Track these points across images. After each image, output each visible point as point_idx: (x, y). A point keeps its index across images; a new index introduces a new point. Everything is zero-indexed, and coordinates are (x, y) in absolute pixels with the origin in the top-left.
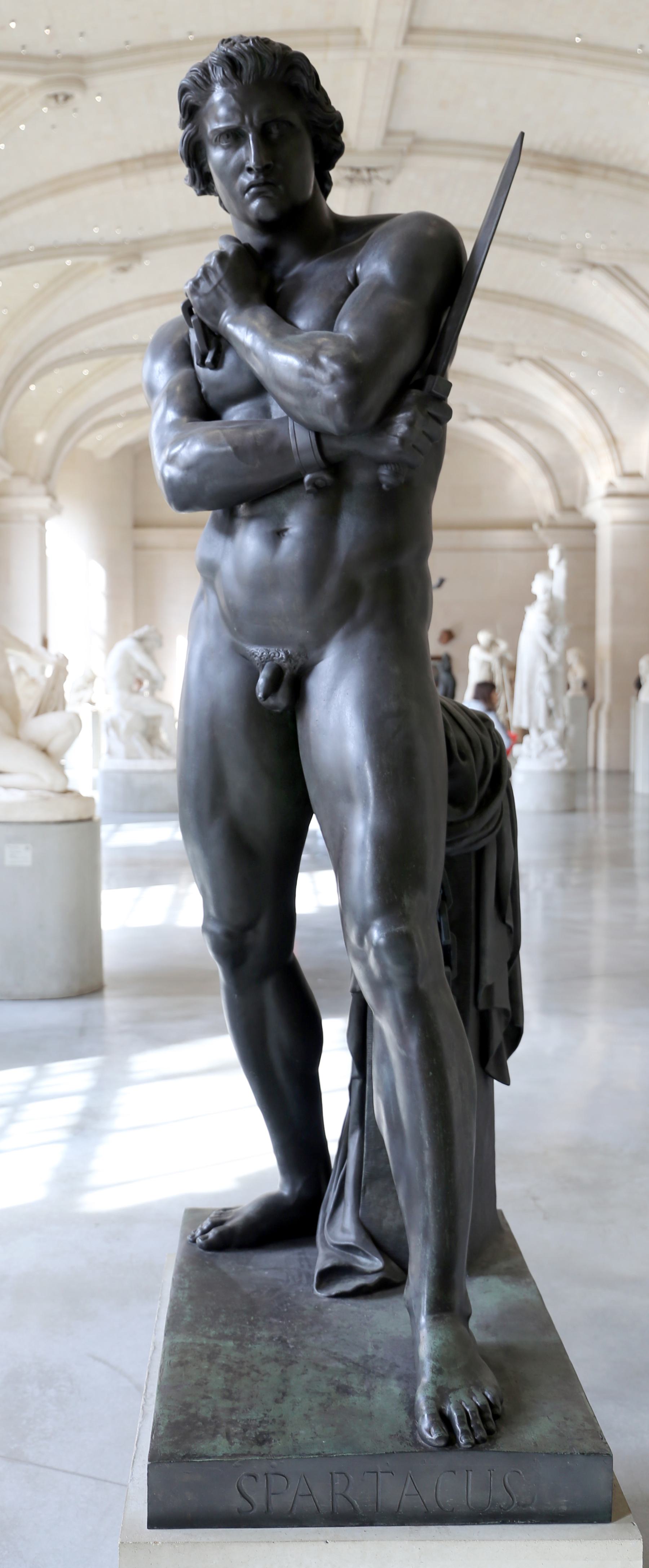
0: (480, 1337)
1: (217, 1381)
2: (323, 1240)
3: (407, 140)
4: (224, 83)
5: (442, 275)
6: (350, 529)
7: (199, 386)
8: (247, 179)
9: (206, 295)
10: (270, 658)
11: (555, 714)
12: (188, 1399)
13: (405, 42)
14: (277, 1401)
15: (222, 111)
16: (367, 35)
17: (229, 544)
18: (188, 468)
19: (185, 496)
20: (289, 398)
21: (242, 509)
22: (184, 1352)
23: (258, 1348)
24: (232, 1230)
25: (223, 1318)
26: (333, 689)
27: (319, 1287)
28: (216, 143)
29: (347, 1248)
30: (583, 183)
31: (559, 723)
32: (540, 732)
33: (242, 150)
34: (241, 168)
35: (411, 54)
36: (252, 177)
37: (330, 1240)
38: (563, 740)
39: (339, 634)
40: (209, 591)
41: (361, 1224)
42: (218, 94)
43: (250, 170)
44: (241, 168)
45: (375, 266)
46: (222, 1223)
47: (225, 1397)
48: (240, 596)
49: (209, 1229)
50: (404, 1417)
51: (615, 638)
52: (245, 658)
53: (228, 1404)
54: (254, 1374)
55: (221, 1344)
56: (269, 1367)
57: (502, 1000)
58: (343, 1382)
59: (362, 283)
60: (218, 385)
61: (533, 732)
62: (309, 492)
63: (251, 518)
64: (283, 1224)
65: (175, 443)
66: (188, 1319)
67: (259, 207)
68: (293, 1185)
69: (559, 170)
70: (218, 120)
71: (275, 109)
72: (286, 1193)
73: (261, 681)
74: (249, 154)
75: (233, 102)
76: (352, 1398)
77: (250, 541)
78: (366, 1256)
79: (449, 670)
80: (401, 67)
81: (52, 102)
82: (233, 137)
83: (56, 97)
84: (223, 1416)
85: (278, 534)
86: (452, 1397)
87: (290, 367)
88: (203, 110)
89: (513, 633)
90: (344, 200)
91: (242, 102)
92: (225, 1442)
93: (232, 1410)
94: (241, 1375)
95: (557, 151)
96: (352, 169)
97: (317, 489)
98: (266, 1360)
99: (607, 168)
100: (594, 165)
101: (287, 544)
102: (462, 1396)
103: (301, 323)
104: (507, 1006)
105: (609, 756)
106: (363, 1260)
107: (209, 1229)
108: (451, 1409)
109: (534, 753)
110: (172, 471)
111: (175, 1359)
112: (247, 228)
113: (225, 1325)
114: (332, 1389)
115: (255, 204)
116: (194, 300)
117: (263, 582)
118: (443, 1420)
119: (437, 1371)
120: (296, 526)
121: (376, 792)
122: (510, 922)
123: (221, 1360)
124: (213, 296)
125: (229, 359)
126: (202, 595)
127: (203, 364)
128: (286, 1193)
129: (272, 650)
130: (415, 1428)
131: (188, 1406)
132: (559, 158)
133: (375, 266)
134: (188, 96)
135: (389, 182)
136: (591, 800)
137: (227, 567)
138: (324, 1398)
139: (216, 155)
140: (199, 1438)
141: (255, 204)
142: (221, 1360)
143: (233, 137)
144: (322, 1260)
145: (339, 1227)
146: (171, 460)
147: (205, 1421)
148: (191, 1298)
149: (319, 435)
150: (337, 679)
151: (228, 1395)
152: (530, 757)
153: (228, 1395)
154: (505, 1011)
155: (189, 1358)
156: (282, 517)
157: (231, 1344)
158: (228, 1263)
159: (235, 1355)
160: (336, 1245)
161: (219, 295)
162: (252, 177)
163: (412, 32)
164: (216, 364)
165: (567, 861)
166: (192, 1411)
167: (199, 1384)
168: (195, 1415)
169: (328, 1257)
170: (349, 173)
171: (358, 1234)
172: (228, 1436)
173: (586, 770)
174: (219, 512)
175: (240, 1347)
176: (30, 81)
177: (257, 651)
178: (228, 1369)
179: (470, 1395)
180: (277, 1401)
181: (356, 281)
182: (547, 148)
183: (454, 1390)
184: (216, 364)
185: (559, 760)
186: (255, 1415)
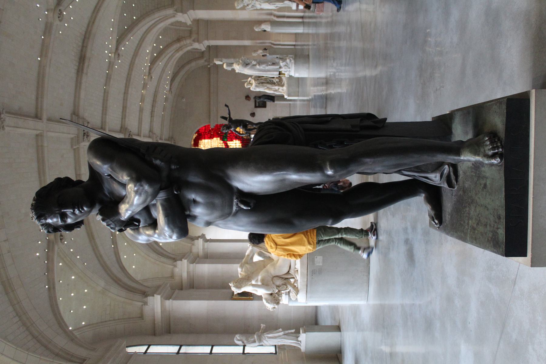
0: (470, 136)
1: (481, 229)
2: (438, 184)
3: (74, 116)
4: (46, 219)
5: (108, 147)
6: (194, 178)
7: (146, 226)
8: (77, 212)
9: (115, 225)
10: (237, 204)
11: (274, 62)
12: (486, 240)
13: (40, 119)
14: (488, 210)
15: (55, 220)
16: (38, 132)
17: (199, 217)
18: (173, 232)
19: (183, 232)
20: (149, 199)
21: (187, 213)
22: (472, 238)
23: (472, 213)
24: (435, 214)
25: (462, 222)
26: (247, 184)
27: (454, 188)
28: (65, 221)
29: (441, 177)
30: (88, 55)
31: (277, 60)
32: (280, 67)
33: (68, 213)
34: (74, 213)
35: (45, 117)
36: (76, 210)
37: (439, 182)
38: (284, 60)
39: (229, 182)
40: (215, 223)
41: (433, 171)
42: (49, 221)
43: (74, 211)
44: (74, 213)
45: (104, 169)
46: (433, 217)
47: (486, 227)
48: (216, 214)
49: (435, 222)
50: (493, 168)
51: (248, 39)
52: (237, 212)
53: (488, 226)
54: (480, 216)
55: (470, 225)
56: (478, 210)
57: (357, 121)
58: (482, 186)
59: (110, 173)
60: (145, 221)
61: (280, 70)
62: (180, 192)
63: (190, 210)
64: (434, 197)
65: (165, 235)
66: (462, 234)
67: (87, 207)
68: (421, 192)
69: (84, 64)
70: (58, 221)
71: (56, 199)
72: (424, 195)
73: (245, 208)
74: (69, 211)
75: (52, 216)
76: (488, 184)
77: (198, 211)
78: (444, 170)
79: (260, 97)
80: (49, 120)
81: (63, 240)
82: (64, 216)
83: (61, 239)
84: (492, 229)
85: (195, 201)
86: (487, 152)
87: (138, 199)
88: (55, 225)
89: (247, 76)
90: (85, 177)
91: (52, 214)
92: (499, 230)
93: (490, 225)
94: (480, 220)
95: (77, 64)
96: (84, 136)
97: (179, 189)
98: (475, 210)
99: (83, 46)
100: (82, 50)
101: (199, 199)
102: (487, 148)
103: (124, 193)
104: (359, 119)
105: (290, 41)
106: (445, 172)
107: (435, 222)
108: (491, 153)
109: (288, 70)
110: (175, 237)
111: (474, 241)
112: (94, 210)
113: (464, 222)
114: (485, 190)
115: (85, 209)
116: (117, 228)
117: (210, 206)
118: (493, 156)
119: (478, 155)
120: (192, 196)
121: (281, 171)
122: (330, 119)
123: (475, 226)
124: (116, 223)
125: (137, 217)
126: (217, 225)
127: (139, 225)
128: (424, 195)
129: (234, 204)
130: (497, 165)
131: (488, 240)
132: (80, 63)
133: (104, 169)
134: (50, 230)
135: (88, 123)
136: (305, 47)
137: (207, 218)
138: (488, 194)
139: (69, 221)
140: (498, 238)
141: (85, 209)
142: (475, 226)
143: (64, 216)
144: (445, 186)
145: (435, 178)
146: (171, 237)
147: (493, 235)
148: (456, 232)
149: (161, 189)
150: (243, 182)
151: (486, 225)
152: (290, 71)
153: (486, 225)
154: (361, 120)
155: (474, 237)
156: (189, 200)
157: (470, 221)
158: (447, 217)
159: (474, 221)
160: (440, 180)
161: (115, 221)
162: (76, 210)
163: (37, 117)
164: (139, 221)
165: (327, 58)
166: (490, 239)
167: (482, 235)
168: (491, 238)
169: (444, 184)
170: (85, 137)
171: (436, 173)
172: (498, 228)
173: (295, 48)
174: (188, 220)
175: (472, 219)
176: (56, 248)
177: (234, 208)
178: (478, 224)
179: (487, 145)
180: (488, 210)
181: (109, 175)
182: (76, 68)
183: (485, 151)
184: (139, 221)
185: (290, 61)
186: (492, 218)
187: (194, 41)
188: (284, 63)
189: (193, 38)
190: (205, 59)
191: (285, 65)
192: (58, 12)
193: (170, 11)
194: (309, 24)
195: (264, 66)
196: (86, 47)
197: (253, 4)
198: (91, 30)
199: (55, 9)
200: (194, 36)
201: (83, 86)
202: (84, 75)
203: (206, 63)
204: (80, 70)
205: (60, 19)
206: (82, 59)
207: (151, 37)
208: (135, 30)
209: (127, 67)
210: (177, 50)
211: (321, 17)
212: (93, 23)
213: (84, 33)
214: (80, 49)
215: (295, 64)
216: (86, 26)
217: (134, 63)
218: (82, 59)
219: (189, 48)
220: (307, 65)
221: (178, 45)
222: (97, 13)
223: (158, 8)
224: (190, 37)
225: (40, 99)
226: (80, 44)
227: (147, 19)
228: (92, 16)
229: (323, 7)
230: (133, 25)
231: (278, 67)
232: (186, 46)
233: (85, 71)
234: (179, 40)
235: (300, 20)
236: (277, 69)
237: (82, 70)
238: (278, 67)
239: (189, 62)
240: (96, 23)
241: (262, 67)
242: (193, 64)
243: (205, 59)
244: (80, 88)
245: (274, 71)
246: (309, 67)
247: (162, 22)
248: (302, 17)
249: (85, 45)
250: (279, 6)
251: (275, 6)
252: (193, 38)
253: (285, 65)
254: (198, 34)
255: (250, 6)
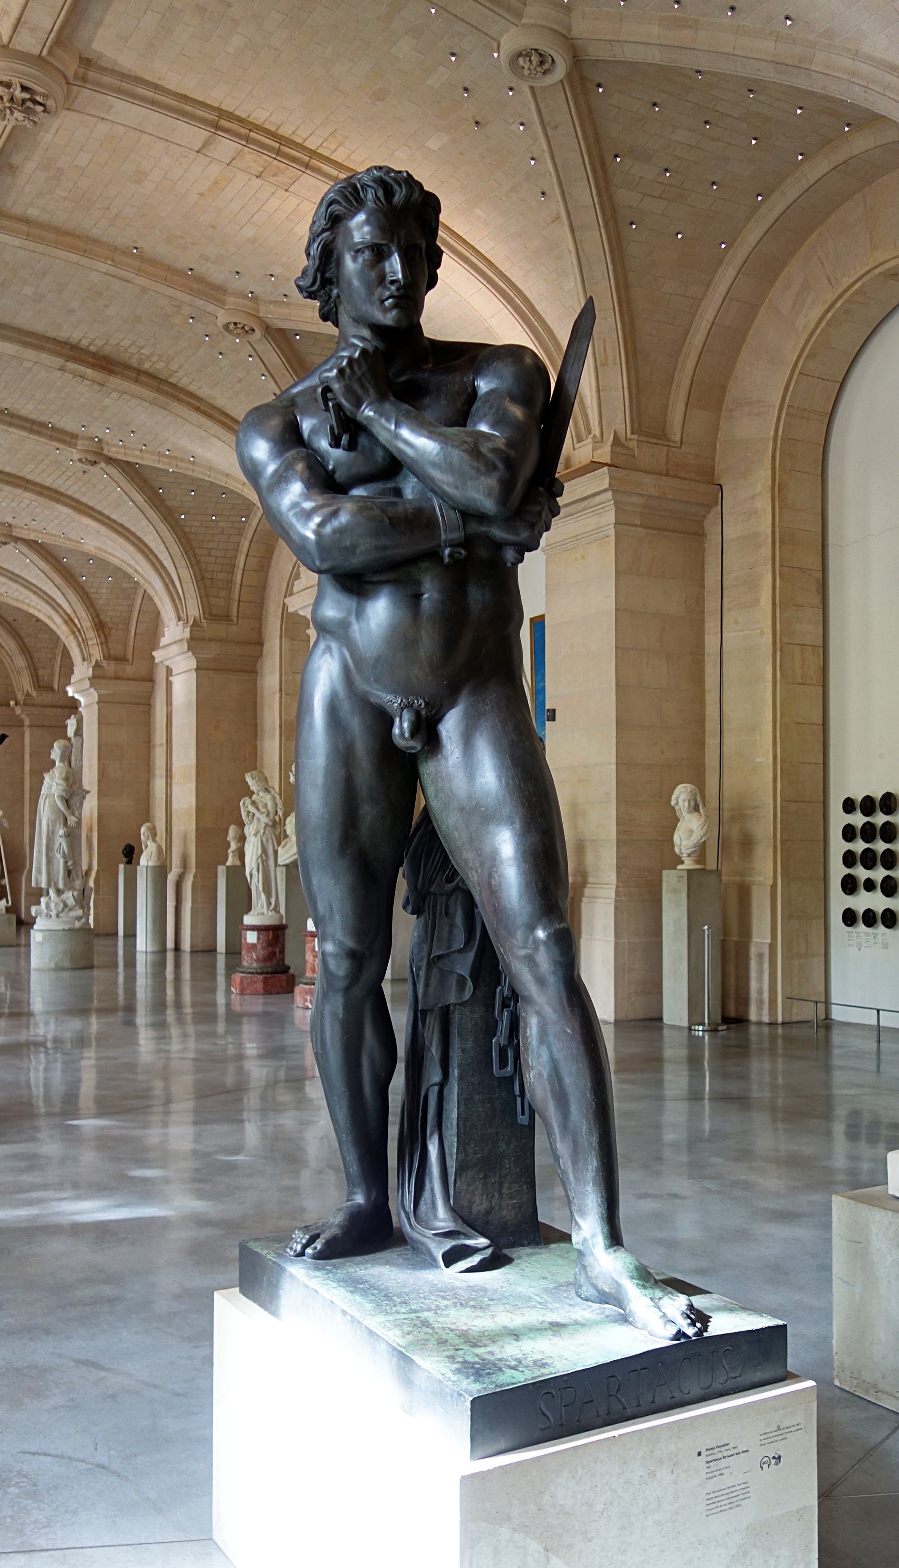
30: (115, 381)
31: (78, 883)
32: (59, 892)
61: (52, 893)
69: (93, 366)
99: (139, 371)
109: (54, 913)
132: (94, 355)
187: (97, 666)
188: (71, 901)
189: (105, 664)
190: (34, 694)
191: (66, 905)
192: (250, 323)
193: (194, 609)
194: (159, 966)
195: (64, 845)
196: (136, 381)
197: (257, 814)
198: (179, 400)
199: (259, 318)
200: (110, 668)
201: (31, 354)
202: (60, 361)
203: (20, 697)
204: (73, 352)
205: (232, 326)
206: (106, 364)
207: (120, 553)
208: (151, 513)
209: (48, 482)
210: (69, 621)
211: (228, 992)
212: (197, 409)
213: (173, 380)
214: (134, 362)
215: (71, 930)
216: (191, 388)
217: (58, 501)
218: (106, 364)
219: (76, 654)
220: (67, 964)
221: (85, 620)
222: (223, 424)
223: (203, 579)
224: (108, 657)
225: (25, 228)
226: (147, 366)
227: (176, 550)
228: (214, 407)
229: (255, 993)
230: (168, 514)
231: (61, 885)
232: (83, 644)
233: (71, 365)
234: (100, 626)
235: (170, 944)
236: (56, 884)
237: (76, 360)
238: (61, 885)
239: (26, 651)
240: (195, 416)
241: (61, 842)
242: (20, 662)
243: (34, 694)
244: (26, 344)
245: (49, 874)
246: (63, 969)
247: (166, 585)
248: (177, 948)
249: (143, 378)
250: (254, 880)
251: (255, 872)
252: (105, 664)
253: (66, 905)
254: (117, 678)
255: (252, 809)
